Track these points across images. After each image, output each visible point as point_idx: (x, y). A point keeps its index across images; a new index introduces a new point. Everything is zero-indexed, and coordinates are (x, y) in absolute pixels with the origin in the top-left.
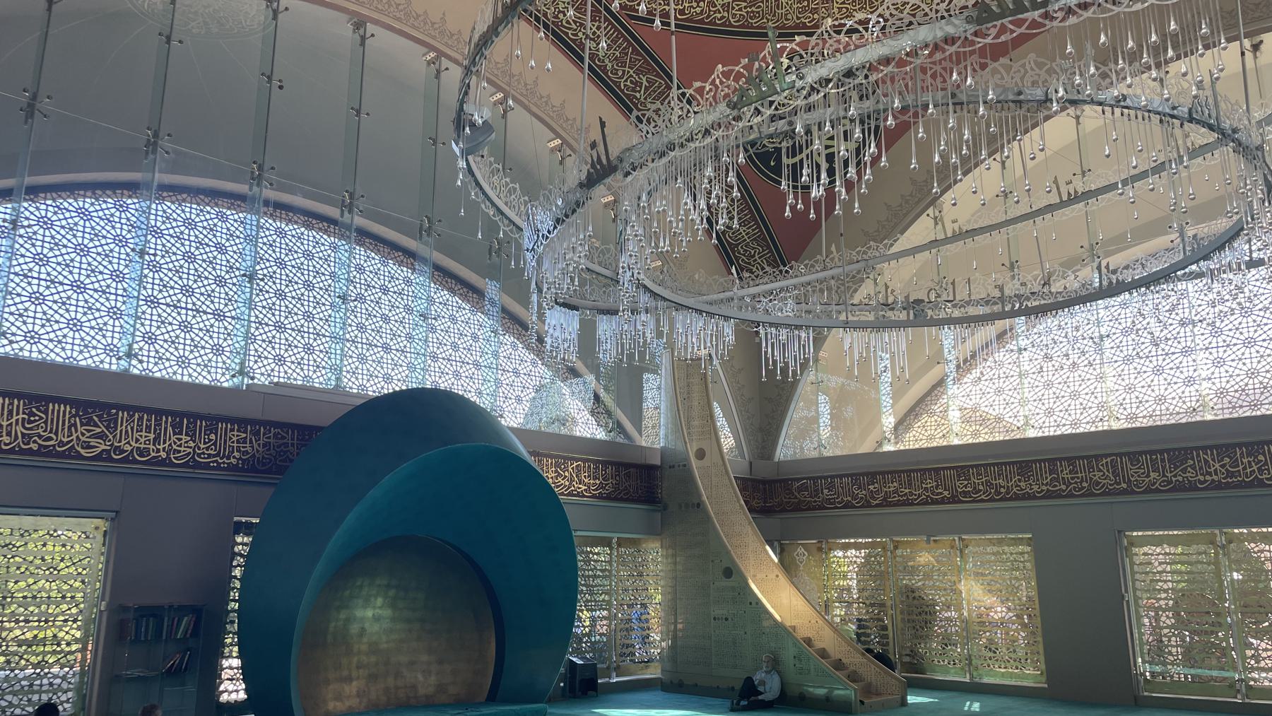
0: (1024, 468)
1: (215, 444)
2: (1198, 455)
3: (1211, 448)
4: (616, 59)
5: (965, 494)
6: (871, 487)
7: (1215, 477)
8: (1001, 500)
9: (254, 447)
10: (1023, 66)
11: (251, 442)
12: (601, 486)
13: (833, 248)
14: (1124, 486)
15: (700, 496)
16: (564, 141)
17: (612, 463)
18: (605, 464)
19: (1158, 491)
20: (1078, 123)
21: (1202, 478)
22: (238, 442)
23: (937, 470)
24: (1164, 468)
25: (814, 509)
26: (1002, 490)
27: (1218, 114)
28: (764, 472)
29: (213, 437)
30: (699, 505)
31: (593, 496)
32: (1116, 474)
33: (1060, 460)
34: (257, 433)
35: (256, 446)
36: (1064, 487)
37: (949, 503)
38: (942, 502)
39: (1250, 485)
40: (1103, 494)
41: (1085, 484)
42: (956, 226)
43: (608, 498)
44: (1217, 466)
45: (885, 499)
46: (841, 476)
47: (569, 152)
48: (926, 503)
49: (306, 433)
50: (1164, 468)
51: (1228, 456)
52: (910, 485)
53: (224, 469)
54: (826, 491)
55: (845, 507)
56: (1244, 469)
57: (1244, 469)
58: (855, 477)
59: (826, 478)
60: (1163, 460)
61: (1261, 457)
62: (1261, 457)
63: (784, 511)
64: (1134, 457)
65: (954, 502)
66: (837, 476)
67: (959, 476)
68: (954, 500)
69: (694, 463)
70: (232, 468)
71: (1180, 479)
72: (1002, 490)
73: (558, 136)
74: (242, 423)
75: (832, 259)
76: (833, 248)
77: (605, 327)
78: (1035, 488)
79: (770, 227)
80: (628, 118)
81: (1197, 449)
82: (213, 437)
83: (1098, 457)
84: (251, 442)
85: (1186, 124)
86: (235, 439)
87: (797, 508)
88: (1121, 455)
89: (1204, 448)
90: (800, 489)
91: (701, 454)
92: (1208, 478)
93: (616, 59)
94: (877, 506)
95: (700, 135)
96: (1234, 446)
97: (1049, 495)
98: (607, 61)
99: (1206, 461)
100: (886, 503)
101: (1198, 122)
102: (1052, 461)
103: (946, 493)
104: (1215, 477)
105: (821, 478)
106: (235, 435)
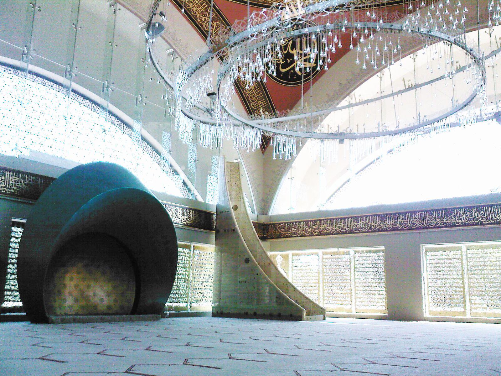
0: (383, 217)
1: (4, 181)
2: (457, 211)
3: (462, 208)
4: (202, 12)
5: (356, 229)
6: (314, 227)
7: (463, 221)
8: (372, 232)
9: (23, 184)
10: (393, 15)
11: (21, 182)
12: (187, 220)
13: (306, 105)
14: (425, 225)
15: (235, 226)
16: (175, 50)
17: (193, 210)
18: (190, 209)
19: (439, 227)
20: (415, 61)
21: (458, 221)
22: (15, 182)
23: (344, 219)
24: (442, 217)
25: (287, 237)
26: (373, 227)
27: (465, 42)
28: (263, 220)
29: (3, 178)
30: (234, 230)
31: (183, 224)
32: (422, 219)
33: (399, 213)
34: (24, 179)
35: (23, 184)
36: (399, 226)
37: (349, 233)
38: (346, 233)
39: (477, 224)
40: (416, 229)
41: (409, 224)
42: (360, 98)
43: (190, 226)
44: (464, 216)
45: (320, 232)
46: (300, 222)
47: (177, 56)
48: (339, 234)
49: (48, 181)
50: (442, 217)
51: (469, 212)
52: (332, 225)
53: (8, 194)
54: (293, 229)
55: (302, 236)
56: (475, 217)
57: (475, 217)
58: (307, 222)
59: (293, 223)
60: (442, 214)
61: (482, 212)
62: (482, 212)
63: (272, 238)
64: (430, 212)
65: (351, 233)
66: (298, 222)
67: (354, 221)
68: (351, 232)
69: (233, 212)
70: (12, 194)
71: (449, 221)
72: (373, 227)
73: (172, 47)
74: (17, 173)
75: (306, 109)
76: (306, 105)
77: (204, 129)
78: (387, 226)
79: (282, 89)
80: (205, 41)
81: (456, 208)
82: (3, 178)
83: (415, 212)
84: (21, 182)
85: (453, 45)
86: (14, 180)
87: (279, 237)
88: (424, 211)
89: (459, 208)
90: (280, 228)
91: (236, 208)
92: (460, 221)
93: (202, 12)
94: (316, 235)
95: (265, 31)
96: (471, 207)
97: (393, 230)
98: (197, 13)
99: (460, 214)
100: (320, 234)
101: (458, 45)
102: (395, 214)
103: (348, 229)
104: (463, 221)
105: (291, 223)
106: (14, 178)
